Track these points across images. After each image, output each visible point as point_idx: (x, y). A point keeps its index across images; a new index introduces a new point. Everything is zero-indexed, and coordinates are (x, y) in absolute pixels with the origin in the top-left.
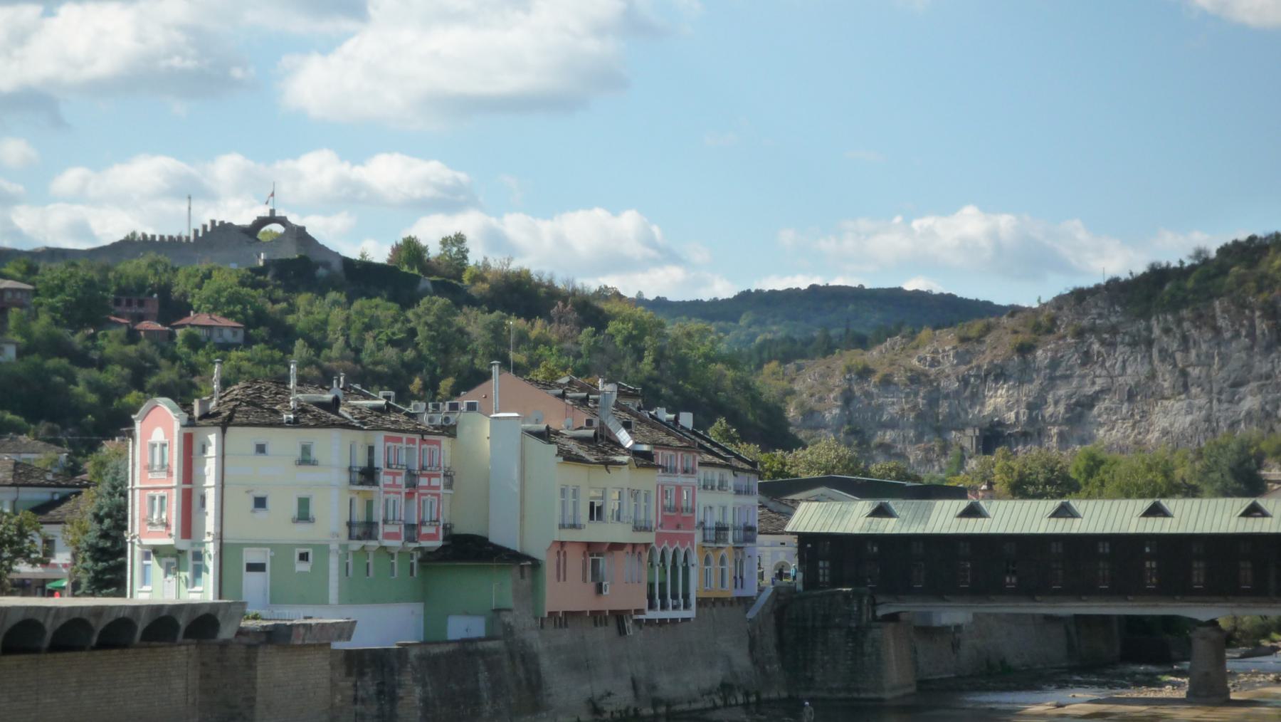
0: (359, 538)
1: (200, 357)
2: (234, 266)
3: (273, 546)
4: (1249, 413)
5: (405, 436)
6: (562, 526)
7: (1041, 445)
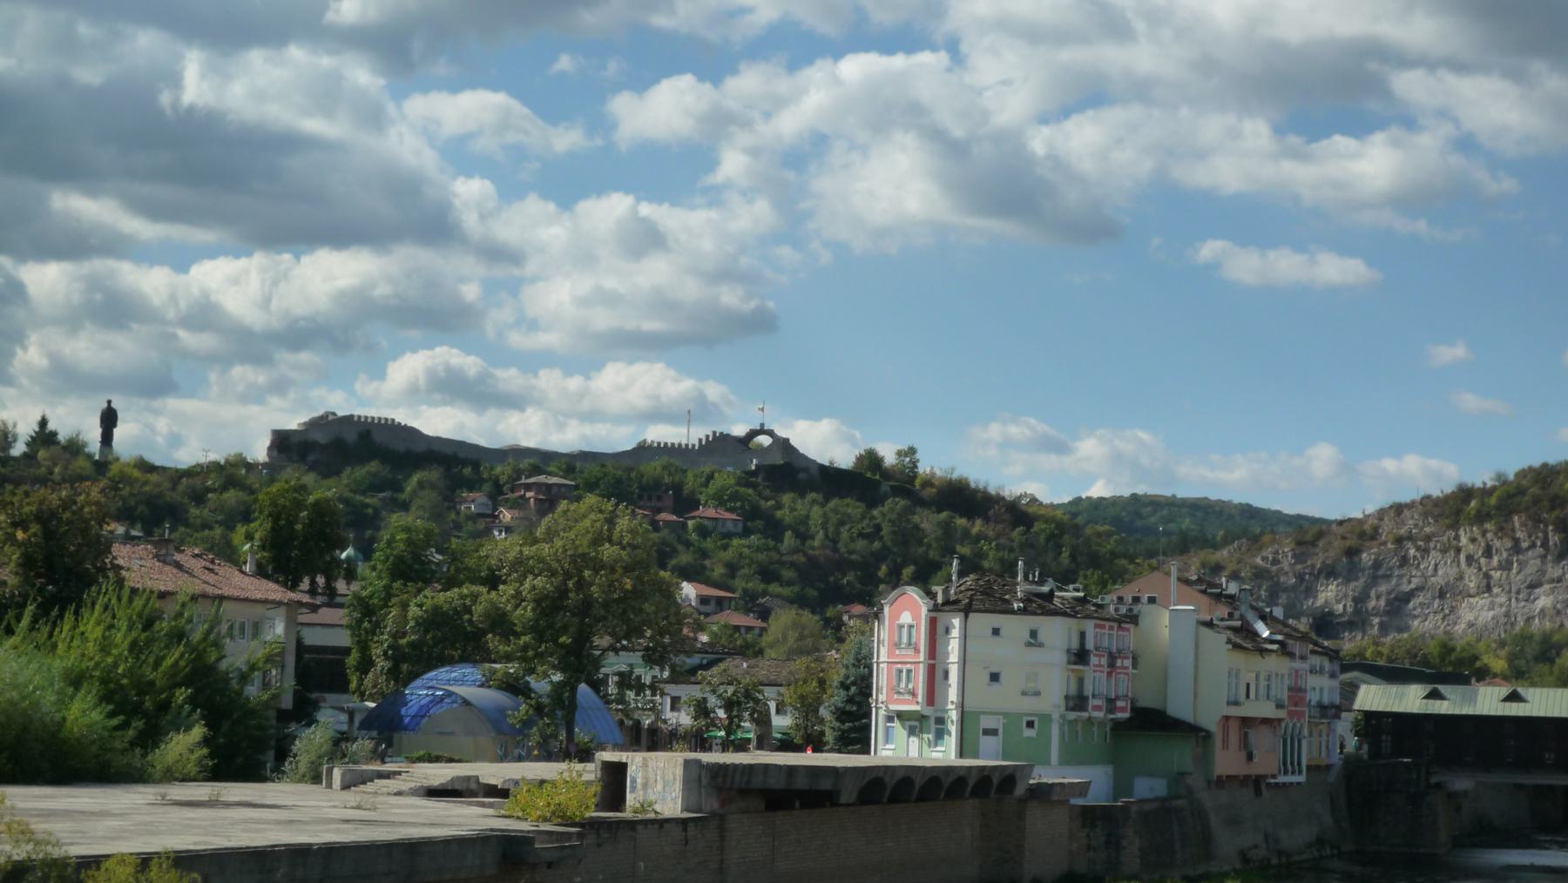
1: (708, 544)
2: (730, 469)
3: (1005, 715)
4: (1542, 610)
5: (1107, 624)
6: (1229, 703)
7: (1364, 633)
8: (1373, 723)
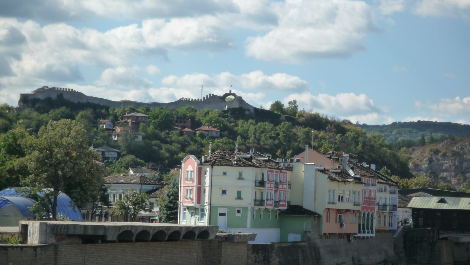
0: (258, 205)
1: (204, 141)
2: (217, 110)
3: (229, 208)
5: (275, 170)
6: (329, 203)
8: (416, 212)
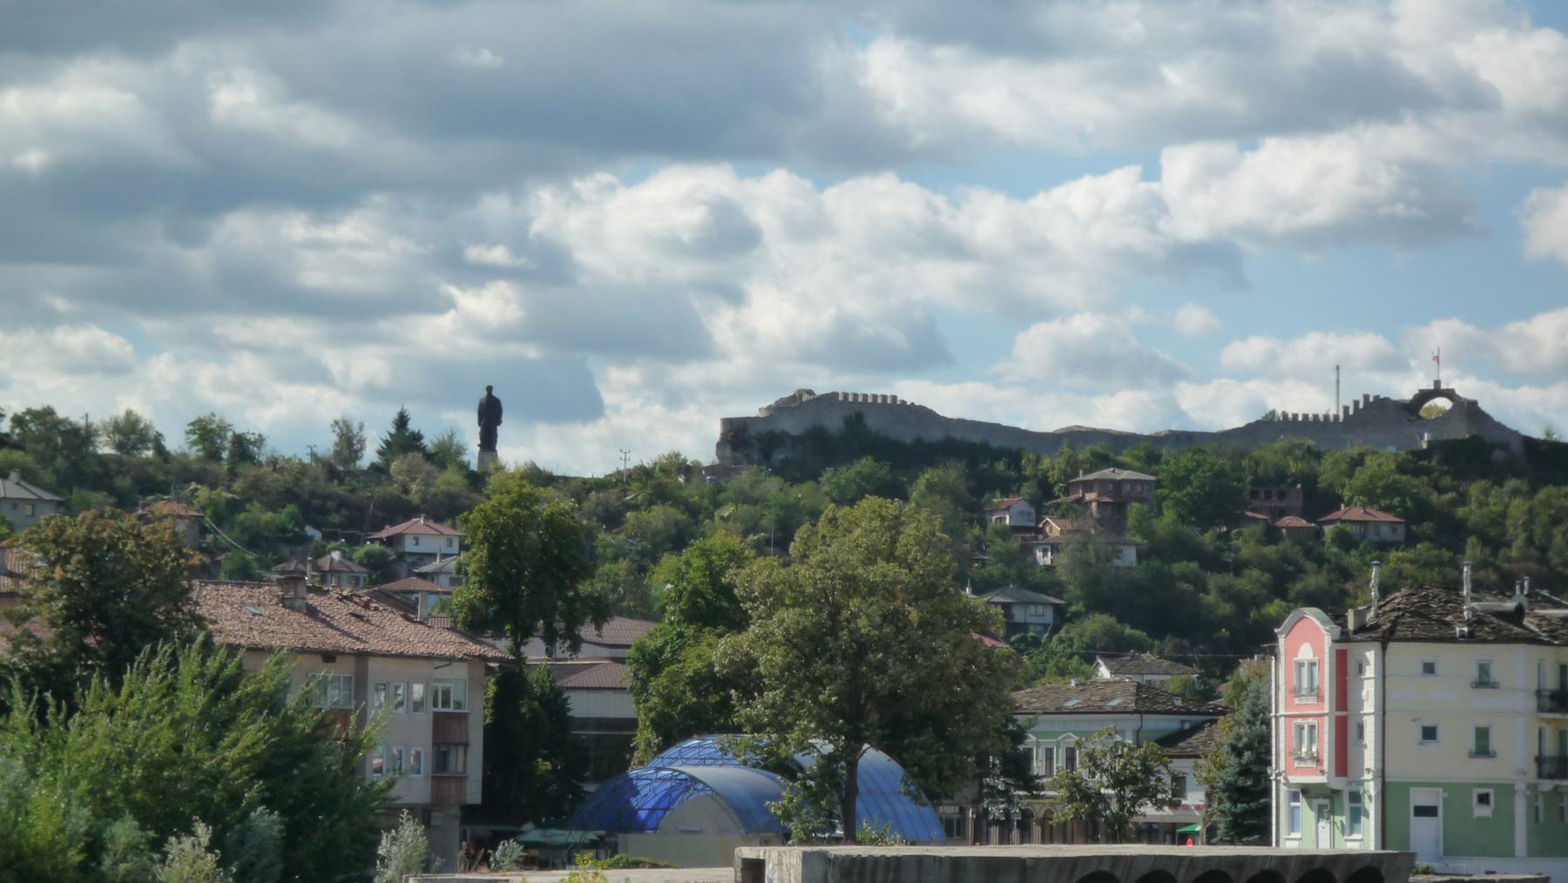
0: (1551, 777)
1: (1352, 559)
2: (1392, 449)
3: (1446, 786)
